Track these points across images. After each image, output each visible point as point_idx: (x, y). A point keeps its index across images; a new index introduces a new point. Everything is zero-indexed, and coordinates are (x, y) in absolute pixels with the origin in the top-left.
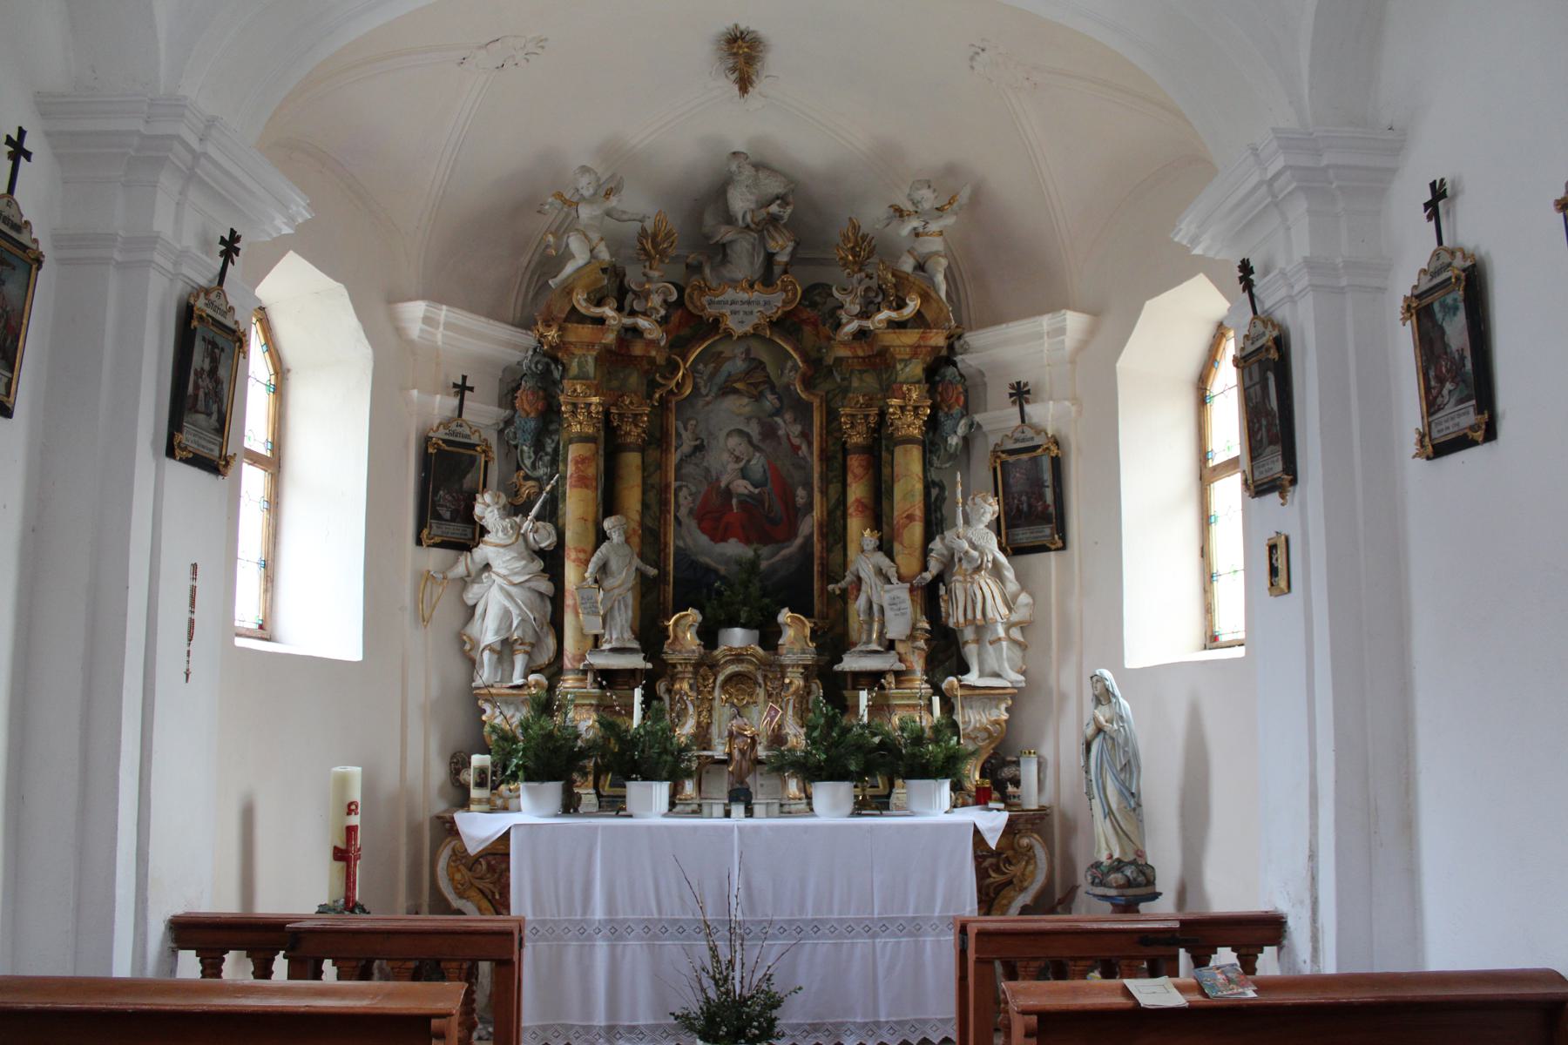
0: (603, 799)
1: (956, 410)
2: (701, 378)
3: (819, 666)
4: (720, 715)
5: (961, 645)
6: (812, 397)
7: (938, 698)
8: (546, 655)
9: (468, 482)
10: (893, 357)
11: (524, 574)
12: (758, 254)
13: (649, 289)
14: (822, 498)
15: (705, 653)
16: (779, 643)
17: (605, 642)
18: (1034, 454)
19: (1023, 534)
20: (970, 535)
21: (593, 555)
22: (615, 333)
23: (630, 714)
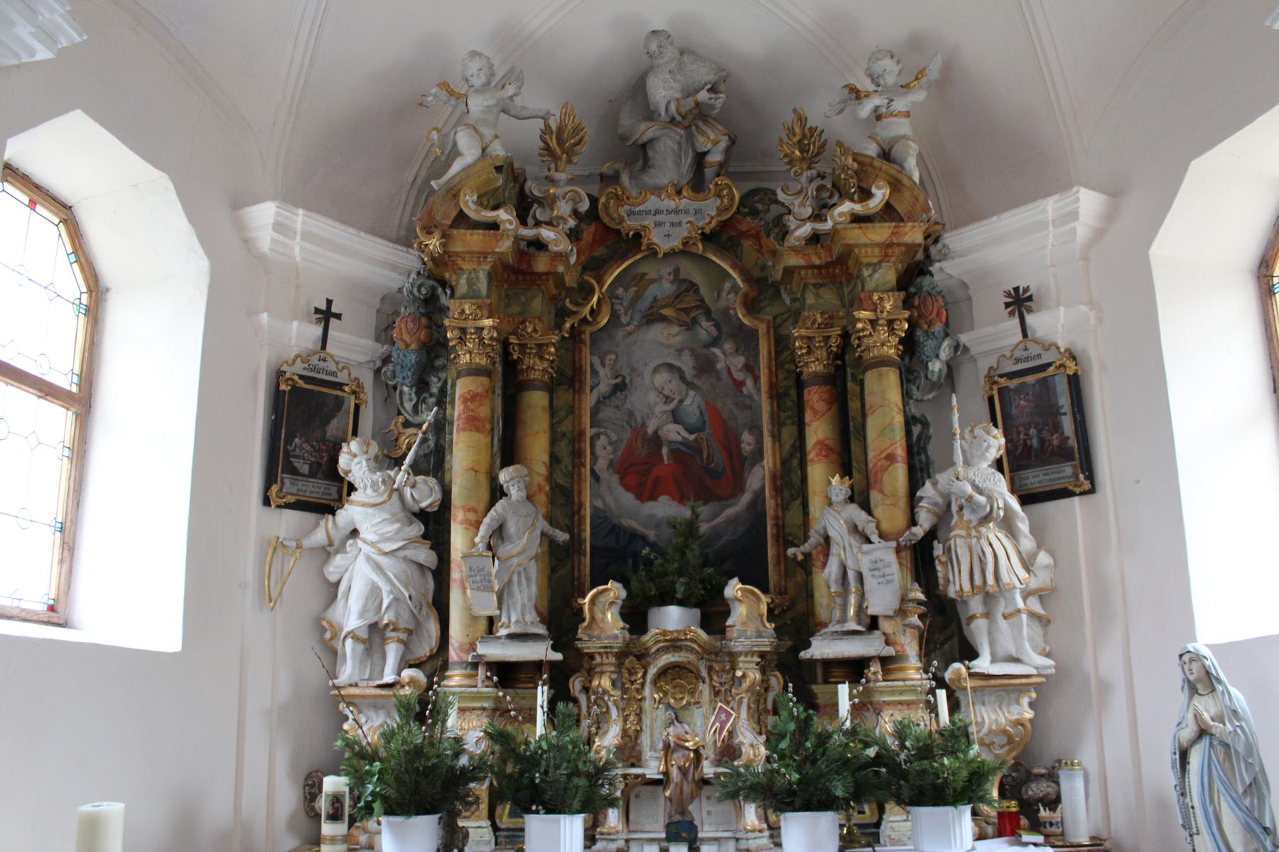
0: (501, 833)
1: (938, 327)
2: (621, 304)
3: (779, 654)
4: (653, 721)
5: (964, 622)
6: (756, 322)
7: (944, 691)
8: (426, 645)
9: (332, 429)
10: (858, 263)
11: (397, 541)
12: (686, 155)
13: (554, 194)
14: (774, 443)
15: (631, 640)
16: (727, 624)
17: (502, 626)
18: (1043, 375)
19: (1034, 477)
20: (971, 475)
21: (486, 516)
22: (512, 239)
23: (533, 719)
